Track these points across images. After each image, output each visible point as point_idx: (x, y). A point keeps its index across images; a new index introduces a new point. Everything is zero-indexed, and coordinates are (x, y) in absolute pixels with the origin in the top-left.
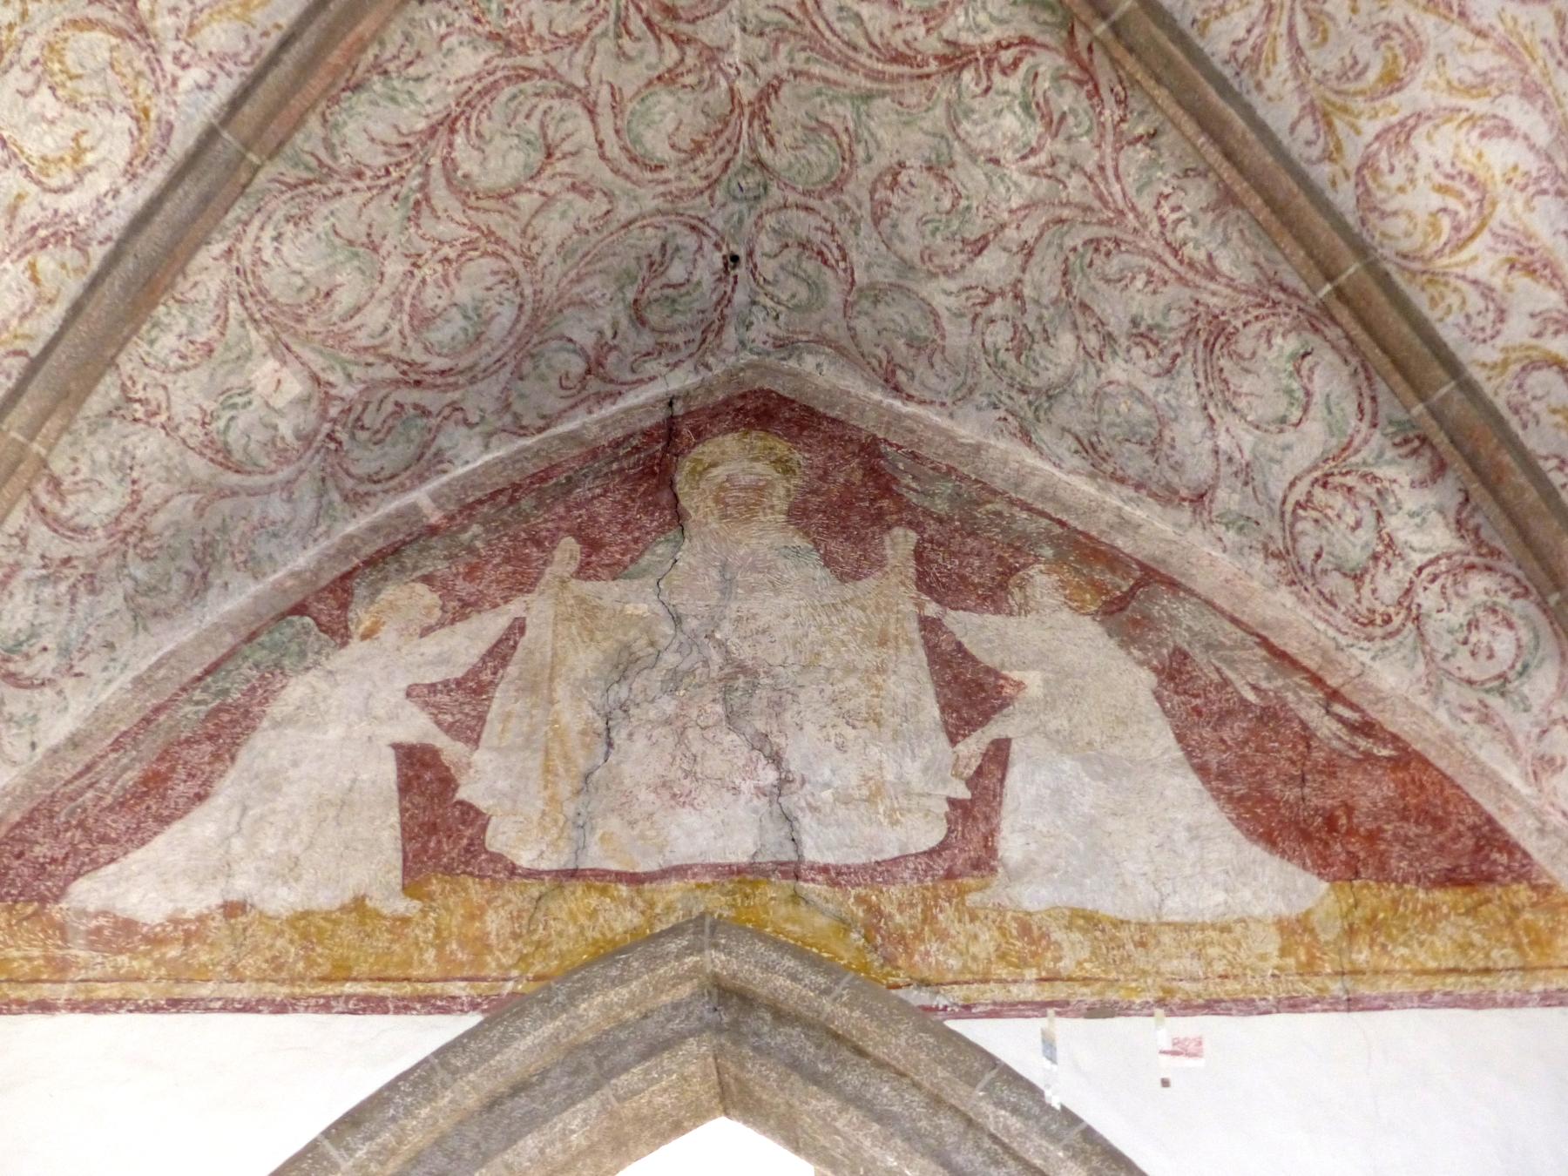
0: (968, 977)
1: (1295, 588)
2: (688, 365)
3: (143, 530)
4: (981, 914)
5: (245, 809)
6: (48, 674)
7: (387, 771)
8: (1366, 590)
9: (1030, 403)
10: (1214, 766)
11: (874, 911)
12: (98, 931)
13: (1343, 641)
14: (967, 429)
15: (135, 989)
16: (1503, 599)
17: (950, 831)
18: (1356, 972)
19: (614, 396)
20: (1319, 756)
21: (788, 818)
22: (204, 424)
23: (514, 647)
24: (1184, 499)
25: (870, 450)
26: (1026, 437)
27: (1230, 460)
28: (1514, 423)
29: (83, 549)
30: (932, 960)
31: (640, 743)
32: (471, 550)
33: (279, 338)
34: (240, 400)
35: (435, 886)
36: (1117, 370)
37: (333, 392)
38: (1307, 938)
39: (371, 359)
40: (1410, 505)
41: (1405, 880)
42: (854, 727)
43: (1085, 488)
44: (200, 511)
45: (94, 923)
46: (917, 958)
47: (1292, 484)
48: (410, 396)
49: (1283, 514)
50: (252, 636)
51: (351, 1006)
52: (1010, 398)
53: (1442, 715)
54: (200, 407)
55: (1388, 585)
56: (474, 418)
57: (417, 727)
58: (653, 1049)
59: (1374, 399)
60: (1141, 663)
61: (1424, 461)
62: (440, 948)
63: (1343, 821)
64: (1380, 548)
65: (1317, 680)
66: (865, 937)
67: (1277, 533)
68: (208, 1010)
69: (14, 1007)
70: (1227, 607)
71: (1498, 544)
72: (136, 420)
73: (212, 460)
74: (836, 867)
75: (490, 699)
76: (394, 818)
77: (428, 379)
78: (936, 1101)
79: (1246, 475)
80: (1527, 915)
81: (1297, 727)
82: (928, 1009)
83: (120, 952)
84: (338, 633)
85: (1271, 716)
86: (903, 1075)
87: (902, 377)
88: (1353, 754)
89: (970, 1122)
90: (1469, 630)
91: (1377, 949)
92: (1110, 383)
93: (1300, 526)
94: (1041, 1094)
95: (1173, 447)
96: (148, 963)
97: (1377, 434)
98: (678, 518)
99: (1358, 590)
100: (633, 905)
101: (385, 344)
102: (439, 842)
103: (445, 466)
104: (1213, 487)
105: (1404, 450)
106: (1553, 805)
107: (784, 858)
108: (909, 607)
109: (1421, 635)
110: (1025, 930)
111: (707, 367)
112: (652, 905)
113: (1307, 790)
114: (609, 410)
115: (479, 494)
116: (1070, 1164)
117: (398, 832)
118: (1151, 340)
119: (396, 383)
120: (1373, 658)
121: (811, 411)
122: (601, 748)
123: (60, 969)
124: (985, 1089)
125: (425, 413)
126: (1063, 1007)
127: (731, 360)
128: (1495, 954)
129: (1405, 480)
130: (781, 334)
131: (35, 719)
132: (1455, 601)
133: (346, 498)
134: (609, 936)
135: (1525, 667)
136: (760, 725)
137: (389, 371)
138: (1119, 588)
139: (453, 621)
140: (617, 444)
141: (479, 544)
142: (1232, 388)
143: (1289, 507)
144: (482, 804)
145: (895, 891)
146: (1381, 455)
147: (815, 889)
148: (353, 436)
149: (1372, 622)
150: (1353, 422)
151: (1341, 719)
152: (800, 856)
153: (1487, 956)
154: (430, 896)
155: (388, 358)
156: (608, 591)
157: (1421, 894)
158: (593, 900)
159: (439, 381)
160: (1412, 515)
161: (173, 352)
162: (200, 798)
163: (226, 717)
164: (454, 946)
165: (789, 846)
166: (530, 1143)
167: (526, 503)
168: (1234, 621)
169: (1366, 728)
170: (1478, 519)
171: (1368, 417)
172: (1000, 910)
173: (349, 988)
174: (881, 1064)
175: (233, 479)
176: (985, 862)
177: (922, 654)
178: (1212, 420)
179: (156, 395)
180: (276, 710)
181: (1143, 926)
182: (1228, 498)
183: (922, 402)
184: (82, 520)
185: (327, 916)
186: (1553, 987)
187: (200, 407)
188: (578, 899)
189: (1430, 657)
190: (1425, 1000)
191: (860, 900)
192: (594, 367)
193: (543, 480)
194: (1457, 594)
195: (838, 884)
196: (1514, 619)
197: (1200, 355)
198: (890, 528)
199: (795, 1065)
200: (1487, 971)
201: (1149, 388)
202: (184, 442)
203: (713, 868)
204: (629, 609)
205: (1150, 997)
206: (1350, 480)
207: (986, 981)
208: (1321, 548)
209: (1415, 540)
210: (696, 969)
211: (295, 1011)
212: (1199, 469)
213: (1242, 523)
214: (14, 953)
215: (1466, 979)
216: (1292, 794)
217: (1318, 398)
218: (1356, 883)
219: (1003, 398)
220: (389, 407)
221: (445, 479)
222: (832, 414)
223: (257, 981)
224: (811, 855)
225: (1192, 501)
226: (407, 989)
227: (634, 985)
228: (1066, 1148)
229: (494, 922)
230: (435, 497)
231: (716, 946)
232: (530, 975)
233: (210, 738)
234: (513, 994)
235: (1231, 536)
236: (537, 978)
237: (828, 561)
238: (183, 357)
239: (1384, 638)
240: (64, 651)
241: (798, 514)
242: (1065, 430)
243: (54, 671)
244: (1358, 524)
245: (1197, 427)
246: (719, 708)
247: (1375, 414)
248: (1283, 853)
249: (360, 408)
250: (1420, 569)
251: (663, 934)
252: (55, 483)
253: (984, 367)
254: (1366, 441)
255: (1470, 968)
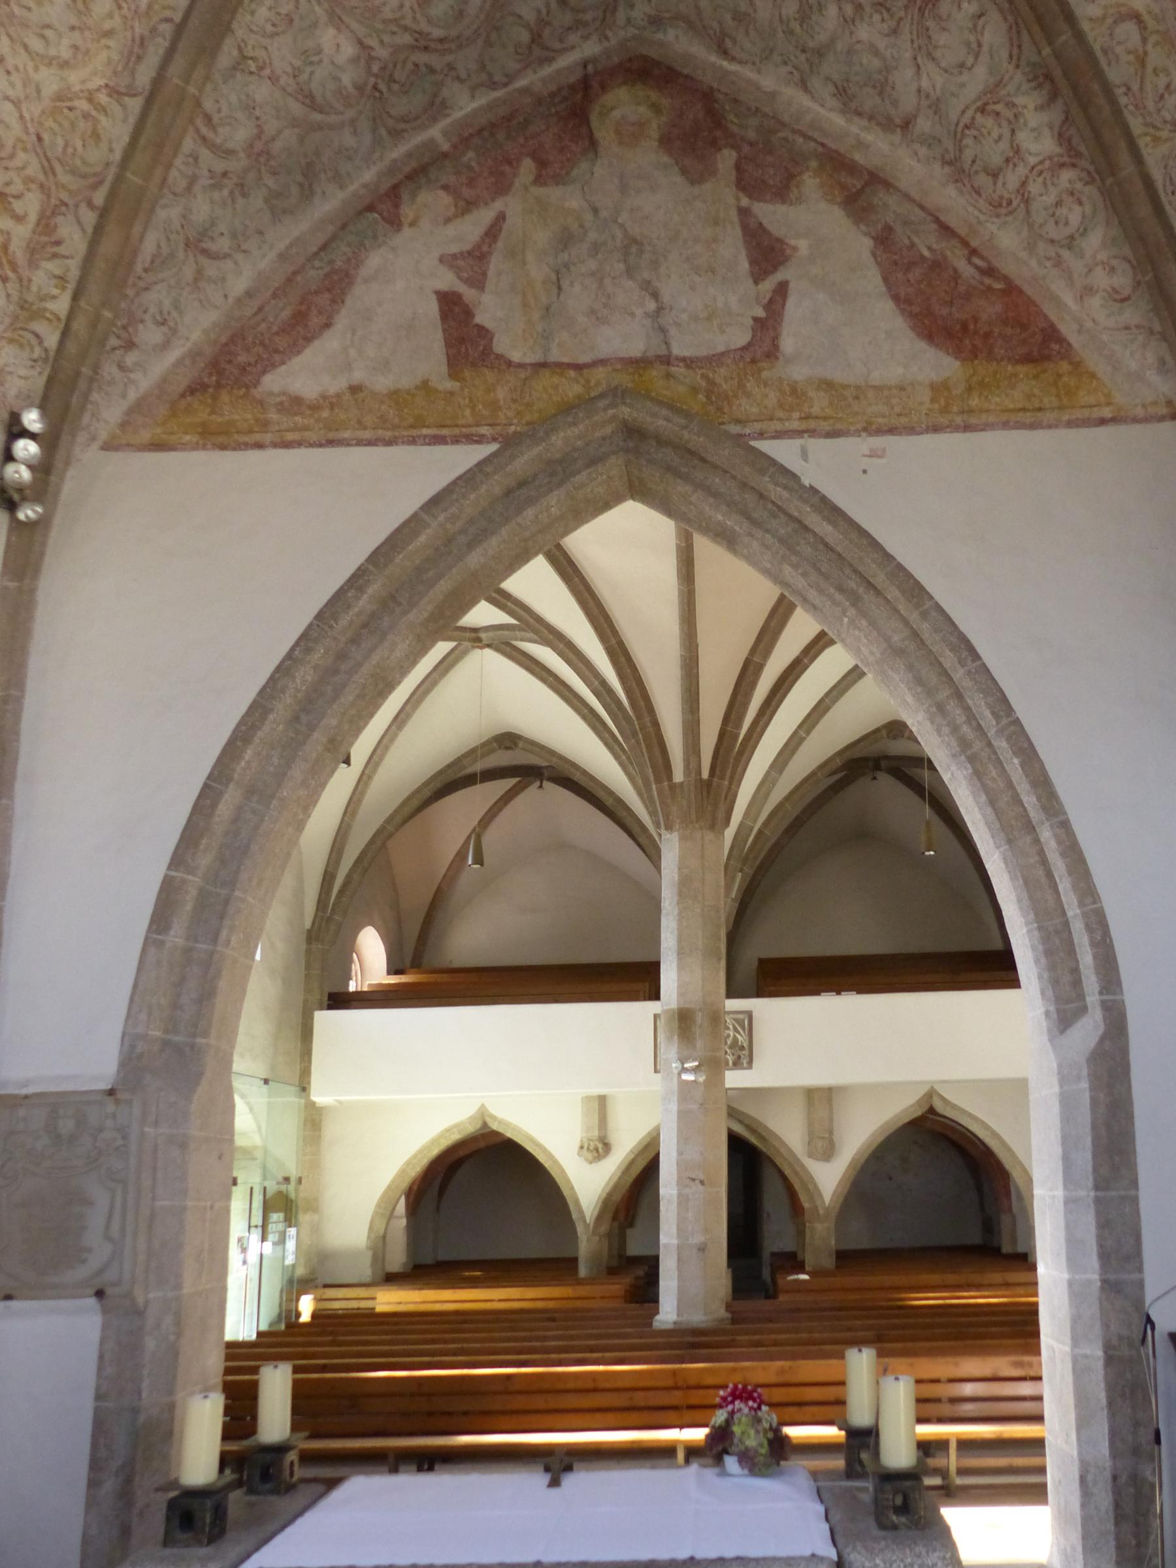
0: (763, 418)
1: (958, 184)
2: (595, 37)
3: (268, 153)
4: (770, 383)
5: (354, 332)
6: (226, 250)
7: (432, 307)
8: (1000, 184)
9: (807, 60)
10: (902, 295)
11: (711, 383)
12: (281, 403)
13: (982, 218)
14: (768, 81)
15: (307, 434)
16: (1079, 186)
17: (753, 336)
18: (971, 411)
19: (550, 60)
20: (962, 289)
21: (663, 330)
22: (295, 76)
23: (500, 231)
24: (897, 126)
25: (708, 97)
26: (804, 85)
27: (927, 96)
28: (1103, 62)
29: (234, 165)
30: (743, 409)
31: (577, 288)
32: (470, 168)
33: (333, 11)
34: (315, 59)
35: (467, 374)
36: (863, 32)
37: (373, 54)
38: (946, 393)
39: (395, 29)
40: (1033, 123)
41: (1002, 360)
42: (700, 276)
43: (839, 121)
44: (301, 140)
45: (278, 400)
46: (734, 408)
47: (963, 112)
48: (423, 58)
49: (956, 132)
50: (344, 227)
51: (427, 441)
52: (796, 57)
53: (1033, 263)
54: (291, 64)
55: (1012, 179)
56: (463, 75)
57: (447, 280)
58: (593, 461)
59: (1019, 47)
60: (865, 234)
61: (1045, 92)
62: (473, 408)
63: (972, 327)
64: (1011, 154)
65: (965, 243)
66: (707, 397)
67: (951, 148)
68: (349, 445)
69: (243, 447)
70: (917, 198)
71: (1082, 148)
72: (251, 73)
73: (303, 103)
74: (690, 358)
75: (489, 262)
76: (440, 335)
77: (432, 45)
78: (744, 485)
79: (936, 107)
80: (1065, 379)
81: (951, 273)
82: (740, 435)
83: (296, 414)
84: (395, 222)
85: (938, 265)
86: (726, 472)
87: (728, 43)
88: (981, 287)
89: (761, 496)
90: (1056, 207)
91: (983, 398)
92: (858, 42)
93: (965, 142)
94: (799, 479)
95: (893, 88)
96: (312, 421)
97: (1019, 72)
98: (593, 144)
99: (995, 184)
100: (578, 382)
101: (403, 17)
102: (467, 349)
103: (448, 111)
104: (915, 117)
105: (1033, 84)
106: (1088, 315)
107: (660, 353)
108: (731, 201)
109: (1028, 212)
110: (794, 391)
111: (606, 38)
112: (588, 381)
113: (954, 309)
114: (547, 70)
115: (470, 131)
116: (813, 514)
117: (443, 343)
118: (886, 8)
119: (413, 48)
120: (999, 229)
121: (671, 69)
122: (555, 290)
123: (264, 425)
124: (770, 477)
125: (432, 71)
126: (813, 433)
127: (622, 33)
128: (1046, 401)
129: (1031, 106)
130: (653, 13)
131: (224, 279)
132: (1051, 188)
133: (390, 133)
134: (566, 399)
135: (1085, 230)
136: (646, 275)
137: (407, 39)
138: (855, 186)
139: (463, 214)
140: (552, 95)
141: (474, 164)
142: (933, 42)
143: (960, 129)
144: (489, 325)
145: (723, 371)
146: (1018, 88)
147: (678, 370)
148: (389, 88)
149: (1000, 205)
150: (1005, 65)
151: (977, 267)
152: (670, 352)
153: (1041, 401)
154: (464, 379)
155: (406, 29)
156: (553, 193)
157: (1010, 368)
158: (556, 379)
159: (439, 47)
160: (1033, 130)
161: (267, 21)
162: (328, 325)
163: (336, 277)
164: (480, 407)
165: (664, 347)
166: (530, 512)
167: (501, 136)
168: (922, 207)
169: (990, 272)
170: (1073, 131)
171: (1014, 61)
172: (780, 379)
173: (425, 431)
174: (715, 467)
175: (318, 117)
176: (773, 353)
177: (738, 231)
178: (918, 66)
179: (260, 54)
180: (364, 272)
181: (858, 388)
182: (924, 124)
183: (740, 62)
184: (230, 145)
185: (408, 392)
186: (1073, 417)
187: (291, 64)
188: (546, 379)
189: (1031, 226)
190: (1005, 425)
191: (703, 376)
192: (536, 38)
193: (509, 120)
194: (1053, 184)
195: (692, 368)
196: (1084, 199)
197: (916, 17)
198: (720, 149)
199: (668, 468)
200: (1040, 409)
201: (881, 44)
202: (284, 89)
203: (621, 360)
204: (567, 204)
205: (859, 426)
206: (998, 107)
207: (771, 419)
208: (976, 156)
209: (1034, 148)
210: (614, 416)
211: (397, 444)
212: (908, 102)
213: (931, 141)
214: (236, 417)
215: (1028, 414)
216: (945, 311)
217: (985, 48)
218: (976, 362)
219: (792, 58)
220: (410, 66)
221: (449, 120)
222: (686, 72)
223: (374, 429)
224: (676, 351)
225: (902, 127)
226: (457, 431)
227: (581, 426)
228: (812, 506)
229: (501, 393)
230: (445, 133)
231: (624, 403)
232: (524, 422)
233: (328, 290)
234: (515, 433)
235: (923, 151)
236: (528, 424)
237: (684, 171)
238: (274, 25)
239: (1006, 215)
240: (234, 235)
241: (665, 141)
242: (828, 79)
243: (230, 248)
244: (1000, 137)
245: (909, 72)
246: (622, 266)
247: (1019, 59)
248: (937, 345)
249: (391, 66)
250: (1033, 168)
251: (595, 398)
252: (208, 118)
253: (780, 35)
254: (1011, 78)
255: (1031, 408)
